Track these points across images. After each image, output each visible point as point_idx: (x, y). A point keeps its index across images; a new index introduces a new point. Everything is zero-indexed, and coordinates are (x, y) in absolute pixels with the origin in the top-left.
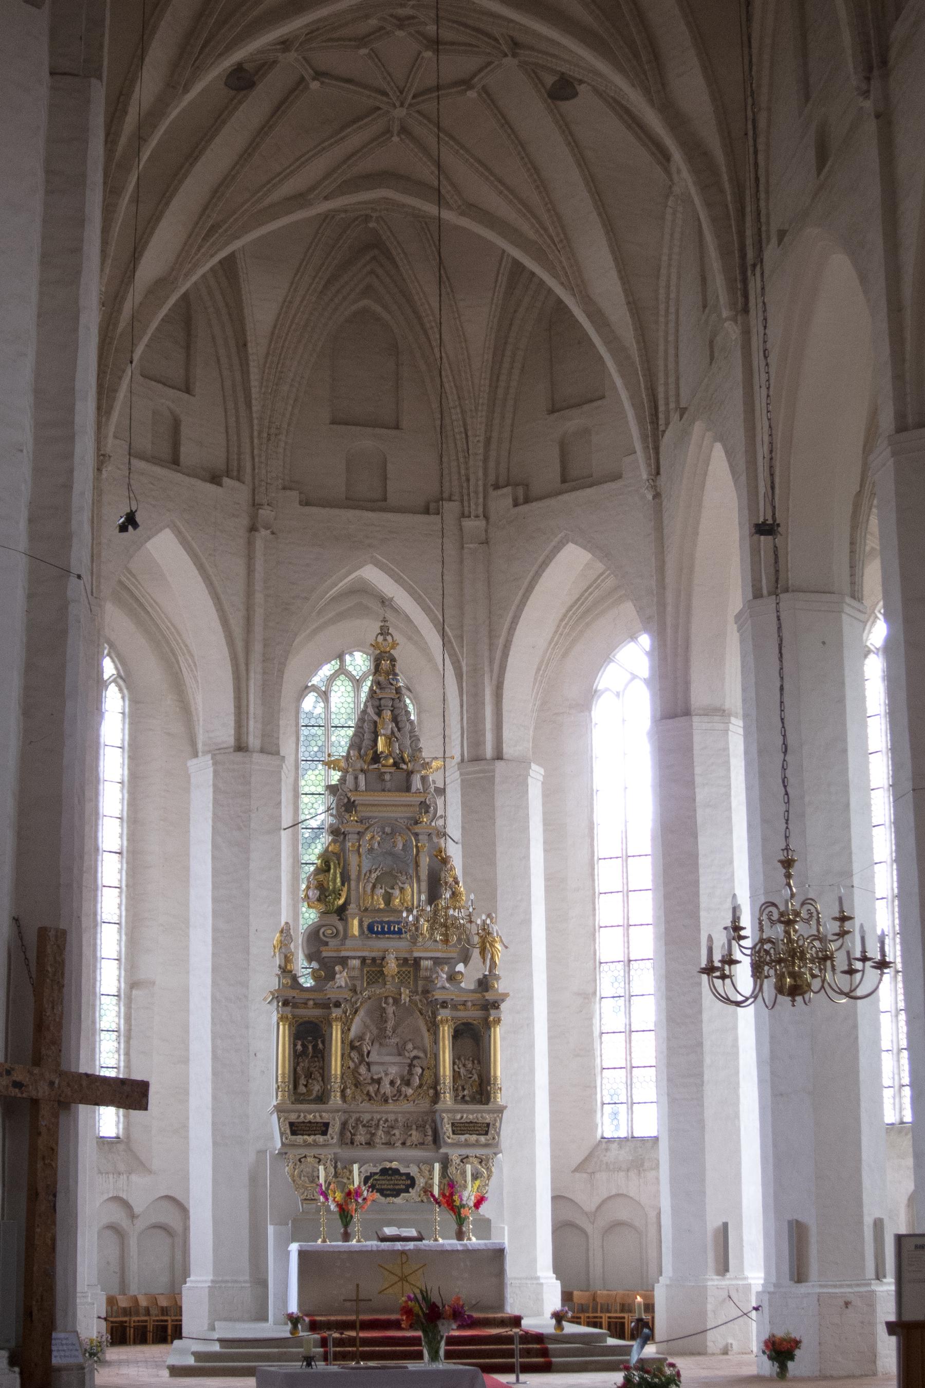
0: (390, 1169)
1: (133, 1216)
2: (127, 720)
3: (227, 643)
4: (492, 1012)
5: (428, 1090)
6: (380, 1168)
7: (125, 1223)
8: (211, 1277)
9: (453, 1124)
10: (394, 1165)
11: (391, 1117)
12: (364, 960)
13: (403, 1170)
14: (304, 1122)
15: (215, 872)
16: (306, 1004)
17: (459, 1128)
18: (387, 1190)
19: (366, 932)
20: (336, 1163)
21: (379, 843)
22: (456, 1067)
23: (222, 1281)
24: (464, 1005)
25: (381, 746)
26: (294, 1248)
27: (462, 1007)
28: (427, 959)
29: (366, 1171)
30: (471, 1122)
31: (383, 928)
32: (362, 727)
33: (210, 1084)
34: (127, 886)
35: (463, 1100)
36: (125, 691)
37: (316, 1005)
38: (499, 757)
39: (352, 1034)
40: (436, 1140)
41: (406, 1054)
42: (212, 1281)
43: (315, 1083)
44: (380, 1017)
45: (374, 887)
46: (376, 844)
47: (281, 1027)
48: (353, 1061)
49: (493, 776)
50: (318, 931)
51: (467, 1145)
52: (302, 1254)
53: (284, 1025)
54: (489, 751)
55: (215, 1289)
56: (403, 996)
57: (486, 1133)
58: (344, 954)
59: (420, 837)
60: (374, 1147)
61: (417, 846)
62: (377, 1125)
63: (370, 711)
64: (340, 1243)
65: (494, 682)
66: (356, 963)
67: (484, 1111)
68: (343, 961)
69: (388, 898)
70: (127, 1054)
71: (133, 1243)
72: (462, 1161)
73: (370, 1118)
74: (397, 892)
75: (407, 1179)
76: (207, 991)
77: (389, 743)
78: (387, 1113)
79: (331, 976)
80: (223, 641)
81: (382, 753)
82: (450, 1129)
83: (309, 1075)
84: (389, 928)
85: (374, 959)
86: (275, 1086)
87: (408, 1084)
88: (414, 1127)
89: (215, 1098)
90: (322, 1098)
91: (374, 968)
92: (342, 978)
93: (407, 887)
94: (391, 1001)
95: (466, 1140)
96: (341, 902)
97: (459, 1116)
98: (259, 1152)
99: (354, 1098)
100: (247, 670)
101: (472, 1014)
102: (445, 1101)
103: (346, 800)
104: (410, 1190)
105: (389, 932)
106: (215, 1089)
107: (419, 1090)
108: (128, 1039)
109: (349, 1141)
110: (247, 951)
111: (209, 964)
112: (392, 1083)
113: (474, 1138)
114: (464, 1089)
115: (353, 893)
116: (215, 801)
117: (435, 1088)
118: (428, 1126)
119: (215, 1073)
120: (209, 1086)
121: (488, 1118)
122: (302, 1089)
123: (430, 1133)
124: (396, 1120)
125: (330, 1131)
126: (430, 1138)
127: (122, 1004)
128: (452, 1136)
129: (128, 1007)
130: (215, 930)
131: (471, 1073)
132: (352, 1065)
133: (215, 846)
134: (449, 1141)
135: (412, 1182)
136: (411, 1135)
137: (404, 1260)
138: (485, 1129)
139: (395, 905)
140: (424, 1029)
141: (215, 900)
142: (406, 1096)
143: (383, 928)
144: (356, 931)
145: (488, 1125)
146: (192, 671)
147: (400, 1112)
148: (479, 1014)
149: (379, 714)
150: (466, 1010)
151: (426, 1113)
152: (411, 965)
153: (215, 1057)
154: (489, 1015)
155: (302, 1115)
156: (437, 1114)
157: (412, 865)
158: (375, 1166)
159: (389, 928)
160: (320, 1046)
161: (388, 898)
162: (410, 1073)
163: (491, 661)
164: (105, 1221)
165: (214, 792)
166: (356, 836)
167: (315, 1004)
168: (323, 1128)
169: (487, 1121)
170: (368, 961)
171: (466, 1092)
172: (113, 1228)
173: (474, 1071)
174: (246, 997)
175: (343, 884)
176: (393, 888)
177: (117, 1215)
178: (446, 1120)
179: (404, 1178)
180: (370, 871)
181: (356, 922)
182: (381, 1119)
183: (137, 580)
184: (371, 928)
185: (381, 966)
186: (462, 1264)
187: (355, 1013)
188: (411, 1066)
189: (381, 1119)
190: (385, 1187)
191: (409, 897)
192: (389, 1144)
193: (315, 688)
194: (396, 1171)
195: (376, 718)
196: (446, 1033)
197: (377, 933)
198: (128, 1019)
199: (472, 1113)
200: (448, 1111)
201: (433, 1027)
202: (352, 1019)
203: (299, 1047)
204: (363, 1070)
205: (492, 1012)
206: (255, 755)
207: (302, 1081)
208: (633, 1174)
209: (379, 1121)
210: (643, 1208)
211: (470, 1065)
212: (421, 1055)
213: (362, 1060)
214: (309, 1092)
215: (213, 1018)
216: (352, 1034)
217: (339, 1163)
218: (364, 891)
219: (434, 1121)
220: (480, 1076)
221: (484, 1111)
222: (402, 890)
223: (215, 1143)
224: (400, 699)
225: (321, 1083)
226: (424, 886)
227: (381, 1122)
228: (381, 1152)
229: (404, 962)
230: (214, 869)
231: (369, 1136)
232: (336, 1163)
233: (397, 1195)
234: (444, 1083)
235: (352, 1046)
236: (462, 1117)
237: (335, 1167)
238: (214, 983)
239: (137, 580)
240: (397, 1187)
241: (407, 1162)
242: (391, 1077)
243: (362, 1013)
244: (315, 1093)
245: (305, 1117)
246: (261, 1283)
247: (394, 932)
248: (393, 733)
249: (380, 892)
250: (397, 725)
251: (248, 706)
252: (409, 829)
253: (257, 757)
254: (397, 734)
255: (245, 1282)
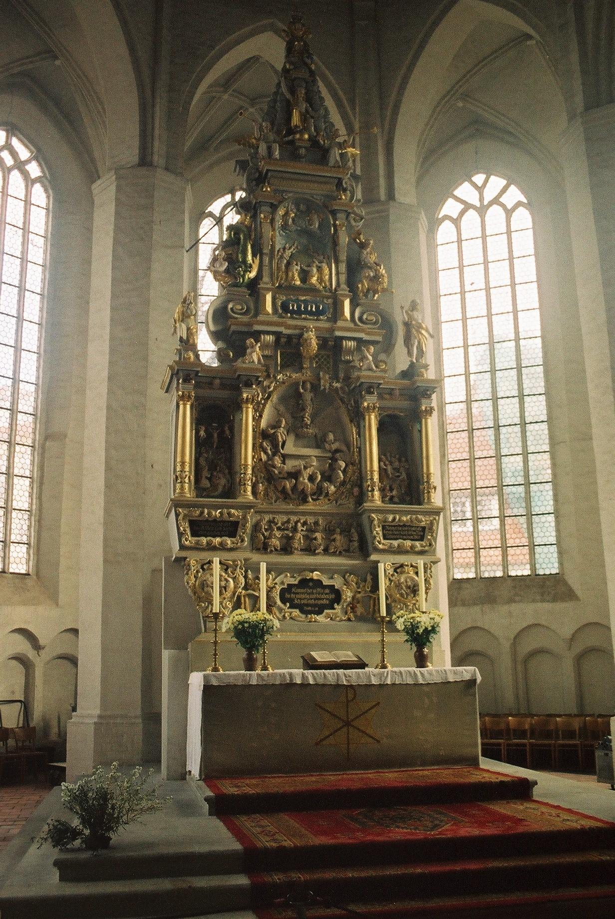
0: (312, 580)
1: (36, 645)
2: (51, 215)
3: (140, 136)
4: (424, 401)
5: (352, 489)
6: (299, 578)
7: (31, 654)
8: (97, 712)
9: (384, 528)
10: (316, 575)
11: (311, 520)
12: (278, 335)
13: (326, 582)
14: (207, 521)
15: (115, 282)
16: (211, 383)
17: (391, 531)
18: (307, 605)
19: (280, 311)
20: (246, 572)
21: (293, 220)
22: (382, 463)
23: (110, 717)
24: (390, 394)
25: (296, 120)
26: (196, 680)
27: (387, 396)
28: (350, 339)
29: (282, 583)
30: (404, 526)
31: (299, 307)
32: (274, 107)
33: (103, 496)
34: (45, 351)
35: (391, 500)
36: (50, 192)
37: (223, 386)
38: (391, 196)
39: (263, 424)
40: (364, 548)
41: (327, 446)
42: (100, 717)
43: (221, 475)
44: (293, 401)
45: (288, 264)
46: (290, 220)
47: (181, 407)
48: (266, 453)
49: (388, 215)
50: (226, 307)
51: (400, 551)
52: (208, 690)
53: (185, 405)
54: (383, 195)
55: (103, 725)
56: (322, 382)
57: (422, 539)
58: (257, 328)
59: (339, 215)
60: (291, 553)
61: (335, 226)
62: (295, 529)
63: (284, 89)
64: (243, 672)
65: (385, 138)
66: (270, 338)
67: (416, 513)
68: (256, 335)
69: (305, 276)
70: (40, 498)
71: (39, 673)
72: (395, 571)
73: (285, 519)
74: (315, 270)
75: (331, 593)
76: (103, 402)
77: (304, 118)
78: (304, 514)
79: (241, 351)
80: (130, 67)
81: (296, 126)
82: (381, 533)
83: (213, 467)
84: (306, 308)
85: (289, 337)
86: (173, 477)
87: (328, 477)
88: (338, 530)
89: (107, 511)
90: (230, 492)
91: (290, 349)
92: (255, 355)
93: (325, 266)
94: (309, 386)
95: (399, 545)
96: (253, 275)
97: (390, 518)
98: (154, 571)
99: (266, 494)
100: (153, 97)
101: (400, 404)
102: (372, 501)
103: (257, 175)
104: (336, 606)
105: (306, 312)
106: (107, 503)
107: (342, 489)
108: (41, 484)
109: (261, 546)
110: (145, 358)
111: (105, 374)
112: (312, 478)
113: (408, 543)
114: (391, 490)
115: (266, 270)
116: (117, 213)
117: (361, 486)
118: (353, 530)
119: (108, 486)
120: (101, 500)
121: (424, 520)
122: (205, 483)
123: (356, 537)
124: (316, 523)
125: (240, 532)
126: (356, 544)
127: (36, 454)
128: (383, 541)
129: (42, 455)
130: (112, 338)
131: (398, 472)
132: (264, 457)
133: (115, 257)
134: (381, 546)
135: (337, 596)
136: (334, 540)
137: (350, 696)
138: (422, 533)
139: (313, 284)
140: (346, 419)
141: (113, 309)
142: (327, 494)
143: (299, 307)
144: (269, 308)
145: (424, 528)
146: (101, 116)
147: (320, 514)
148: (405, 404)
149: (293, 91)
150: (391, 399)
151: (351, 516)
152: (332, 346)
153: (108, 468)
154: (419, 405)
155: (206, 511)
156: (365, 517)
157: (330, 245)
158: (293, 577)
159: (306, 308)
160: (228, 432)
161: (305, 276)
162: (333, 468)
163: (383, 119)
164: (11, 652)
165: (116, 205)
166: (269, 209)
167: (221, 384)
168: (231, 528)
169: (423, 524)
170: (283, 340)
171: (394, 493)
172: (21, 659)
173: (402, 470)
174: (144, 406)
175: (254, 255)
176: (309, 266)
177: (23, 646)
178: (376, 522)
179: (327, 591)
180: (284, 249)
181: (269, 297)
182: (298, 521)
183: (50, 30)
184: (285, 307)
185: (299, 344)
186: (426, 700)
187: (268, 398)
188: (334, 460)
189: (298, 521)
190: (305, 602)
191: (327, 277)
192: (309, 550)
193: (211, 215)
194: (318, 583)
195: (288, 96)
196: (373, 421)
197: (293, 312)
198: (41, 468)
199: (404, 514)
200: (378, 511)
201: (358, 416)
202: (264, 405)
203: (202, 433)
204: (277, 461)
205: (424, 401)
206: (159, 171)
207: (206, 473)
208: (487, 607)
209: (296, 523)
210: (497, 639)
211: (397, 464)
212: (344, 448)
213: (276, 452)
214: (214, 486)
215: (107, 428)
216: (263, 424)
217: (250, 572)
218: (279, 269)
219: (360, 526)
220: (409, 476)
221: (416, 513)
222: (319, 269)
223: (106, 561)
224: (314, 81)
225: (228, 476)
226: (343, 267)
227: (299, 524)
228: (298, 558)
229: (323, 343)
230: (113, 279)
231: (284, 541)
232: (246, 572)
233: (319, 612)
234: (372, 479)
235: (265, 436)
236: (394, 519)
237: (246, 577)
238: (110, 392)
239: (50, 30)
240: (320, 602)
241: (330, 571)
242: (309, 471)
243: (275, 398)
244: (220, 489)
245: (209, 514)
246: (152, 718)
247: (311, 313)
248: (307, 110)
249: (296, 269)
250: (311, 106)
251: (153, 129)
252: (327, 207)
253: (160, 173)
254: (312, 113)
255: (136, 717)
